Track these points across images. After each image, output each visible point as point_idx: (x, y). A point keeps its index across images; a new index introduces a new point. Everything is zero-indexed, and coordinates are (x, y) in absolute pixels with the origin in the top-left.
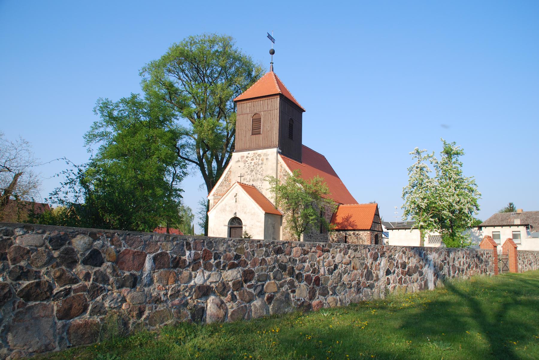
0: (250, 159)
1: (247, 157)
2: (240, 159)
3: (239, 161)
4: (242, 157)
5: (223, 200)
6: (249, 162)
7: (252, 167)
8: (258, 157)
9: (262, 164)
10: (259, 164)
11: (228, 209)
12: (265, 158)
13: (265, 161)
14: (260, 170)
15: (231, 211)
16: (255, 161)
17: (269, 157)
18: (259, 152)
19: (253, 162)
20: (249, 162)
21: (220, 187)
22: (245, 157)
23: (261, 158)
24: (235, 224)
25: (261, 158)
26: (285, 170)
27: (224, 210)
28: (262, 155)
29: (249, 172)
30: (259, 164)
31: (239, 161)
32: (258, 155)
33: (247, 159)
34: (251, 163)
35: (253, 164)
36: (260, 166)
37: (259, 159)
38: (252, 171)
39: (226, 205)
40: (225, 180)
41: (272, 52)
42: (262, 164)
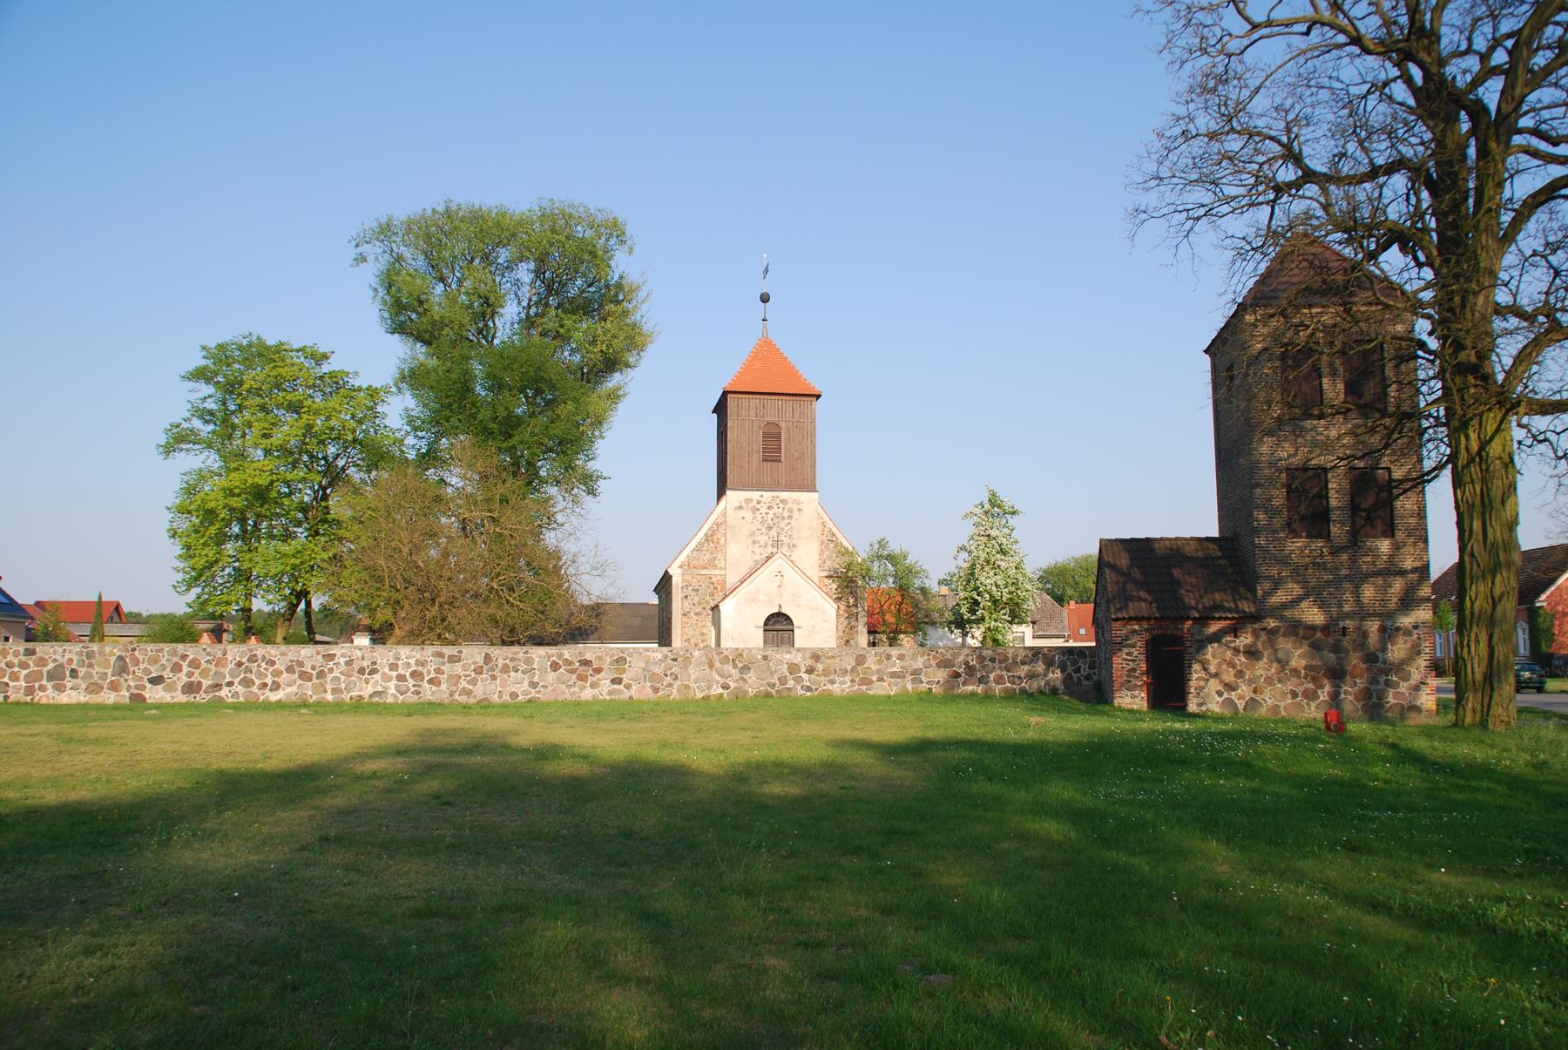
3: (740, 507)
4: (749, 501)
11: (762, 597)
12: (795, 508)
13: (795, 513)
16: (775, 510)
18: (784, 495)
24: (778, 625)
31: (740, 507)
38: (770, 528)
41: (765, 299)
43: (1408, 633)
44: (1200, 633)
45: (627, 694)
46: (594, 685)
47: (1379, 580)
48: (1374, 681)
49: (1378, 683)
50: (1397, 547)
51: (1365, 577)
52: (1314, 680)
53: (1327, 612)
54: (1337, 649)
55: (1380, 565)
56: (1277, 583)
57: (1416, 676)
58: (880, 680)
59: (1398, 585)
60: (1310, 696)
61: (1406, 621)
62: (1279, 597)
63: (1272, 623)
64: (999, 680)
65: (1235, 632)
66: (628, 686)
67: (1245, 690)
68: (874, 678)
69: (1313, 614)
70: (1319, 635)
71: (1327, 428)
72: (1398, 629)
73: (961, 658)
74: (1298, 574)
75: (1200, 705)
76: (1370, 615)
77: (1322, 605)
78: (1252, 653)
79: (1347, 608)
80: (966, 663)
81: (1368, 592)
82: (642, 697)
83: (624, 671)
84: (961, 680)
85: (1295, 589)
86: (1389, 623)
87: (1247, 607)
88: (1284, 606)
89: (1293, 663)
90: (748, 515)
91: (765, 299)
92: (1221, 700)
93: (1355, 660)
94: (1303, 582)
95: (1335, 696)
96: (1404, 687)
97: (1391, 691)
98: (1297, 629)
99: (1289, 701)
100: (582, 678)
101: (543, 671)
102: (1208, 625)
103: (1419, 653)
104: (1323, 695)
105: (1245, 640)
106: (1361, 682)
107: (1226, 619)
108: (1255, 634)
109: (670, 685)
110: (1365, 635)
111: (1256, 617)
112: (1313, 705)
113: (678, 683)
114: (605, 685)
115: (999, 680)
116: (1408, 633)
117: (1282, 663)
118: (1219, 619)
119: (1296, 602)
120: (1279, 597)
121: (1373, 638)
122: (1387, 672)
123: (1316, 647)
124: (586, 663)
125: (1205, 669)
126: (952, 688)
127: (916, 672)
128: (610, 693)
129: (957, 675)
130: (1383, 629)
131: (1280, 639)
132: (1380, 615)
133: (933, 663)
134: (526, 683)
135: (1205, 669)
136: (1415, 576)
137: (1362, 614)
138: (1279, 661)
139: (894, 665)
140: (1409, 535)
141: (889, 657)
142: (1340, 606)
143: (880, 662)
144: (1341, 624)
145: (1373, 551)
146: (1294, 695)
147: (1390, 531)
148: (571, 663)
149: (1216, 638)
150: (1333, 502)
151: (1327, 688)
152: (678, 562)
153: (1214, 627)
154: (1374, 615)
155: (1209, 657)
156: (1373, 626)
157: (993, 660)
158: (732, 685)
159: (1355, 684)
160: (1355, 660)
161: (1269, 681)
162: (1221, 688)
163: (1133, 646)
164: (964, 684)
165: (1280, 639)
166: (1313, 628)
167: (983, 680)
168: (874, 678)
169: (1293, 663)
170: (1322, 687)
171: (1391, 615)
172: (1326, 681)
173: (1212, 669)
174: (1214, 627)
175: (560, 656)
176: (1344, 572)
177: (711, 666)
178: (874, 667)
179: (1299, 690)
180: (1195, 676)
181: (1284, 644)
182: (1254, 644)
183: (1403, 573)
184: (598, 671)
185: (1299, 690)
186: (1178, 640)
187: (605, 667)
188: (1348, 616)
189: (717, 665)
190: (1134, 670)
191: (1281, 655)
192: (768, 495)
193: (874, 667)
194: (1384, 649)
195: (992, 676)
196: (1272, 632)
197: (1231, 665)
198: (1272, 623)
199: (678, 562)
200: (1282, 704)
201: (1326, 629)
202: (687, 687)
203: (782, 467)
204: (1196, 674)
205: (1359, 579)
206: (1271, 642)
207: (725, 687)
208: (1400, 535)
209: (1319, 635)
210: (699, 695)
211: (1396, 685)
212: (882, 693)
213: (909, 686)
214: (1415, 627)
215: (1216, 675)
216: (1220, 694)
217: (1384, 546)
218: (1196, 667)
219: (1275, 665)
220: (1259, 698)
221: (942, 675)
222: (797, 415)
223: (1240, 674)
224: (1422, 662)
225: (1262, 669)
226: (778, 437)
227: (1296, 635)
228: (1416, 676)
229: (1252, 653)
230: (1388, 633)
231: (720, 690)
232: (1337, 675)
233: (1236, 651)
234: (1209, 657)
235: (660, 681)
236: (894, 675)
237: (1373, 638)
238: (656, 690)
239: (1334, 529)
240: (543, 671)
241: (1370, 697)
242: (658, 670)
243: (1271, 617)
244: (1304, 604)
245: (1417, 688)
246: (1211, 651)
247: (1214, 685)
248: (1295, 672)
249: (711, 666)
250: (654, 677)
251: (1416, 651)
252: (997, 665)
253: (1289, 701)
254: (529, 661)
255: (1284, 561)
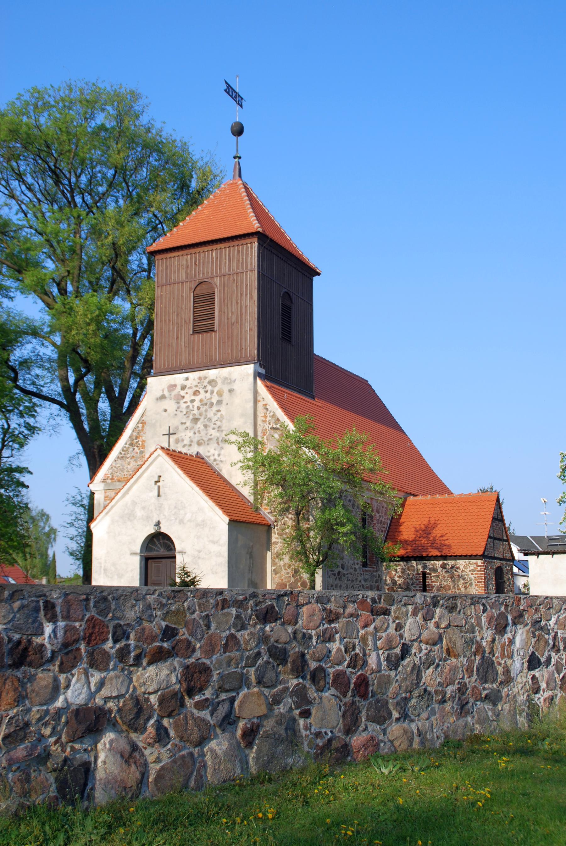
0: (190, 392)
1: (183, 388)
2: (166, 393)
3: (163, 397)
4: (172, 387)
5: (127, 493)
6: (188, 398)
7: (196, 411)
8: (209, 388)
9: (219, 402)
10: (212, 404)
11: (139, 513)
12: (226, 389)
13: (226, 395)
14: (215, 418)
15: (148, 518)
16: (202, 395)
17: (235, 386)
18: (212, 373)
19: (197, 398)
20: (188, 398)
21: (119, 461)
22: (179, 388)
23: (216, 390)
25: (216, 390)
26: (274, 416)
27: (129, 516)
28: (219, 382)
29: (188, 424)
30: (212, 404)
31: (163, 397)
32: (210, 382)
33: (183, 393)
34: (193, 401)
35: (197, 404)
36: (215, 408)
37: (212, 392)
39: (134, 503)
40: (131, 444)
41: (238, 131)
42: (219, 402)
90: (170, 405)
91: (238, 131)
192: (193, 376)
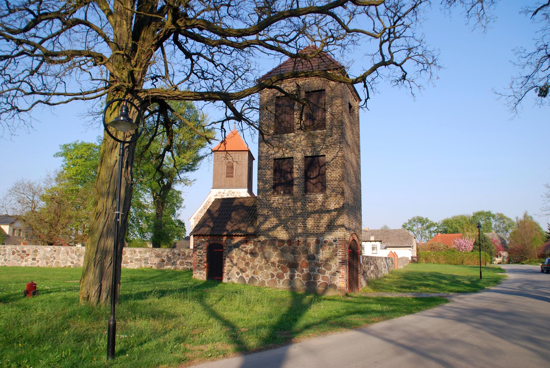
43: (331, 244)
44: (230, 242)
45: (36, 265)
46: (26, 261)
47: (317, 216)
48: (312, 270)
49: (315, 271)
50: (326, 197)
51: (309, 214)
52: (282, 268)
53: (289, 233)
54: (293, 252)
55: (317, 208)
56: (266, 218)
57: (334, 268)
58: (131, 262)
59: (326, 219)
60: (280, 277)
61: (329, 238)
62: (267, 225)
63: (262, 238)
64: (182, 264)
65: (246, 242)
66: (38, 261)
67: (249, 273)
68: (129, 261)
69: (282, 234)
70: (286, 244)
71: (295, 137)
72: (325, 242)
73: (165, 253)
74: (276, 212)
75: (229, 279)
76: (311, 234)
77: (286, 228)
78: (253, 254)
79: (300, 231)
80: (167, 256)
81: (310, 223)
82: (42, 266)
83: (36, 255)
84: (165, 263)
85: (274, 221)
86: (321, 239)
87: (251, 230)
88: (269, 230)
89: (272, 260)
92: (238, 277)
93: (302, 259)
94: (278, 217)
95: (292, 277)
96: (328, 274)
97: (321, 275)
98: (274, 241)
99: (270, 279)
100: (22, 258)
101: (9, 254)
102: (232, 239)
103: (336, 255)
104: (286, 277)
105: (250, 247)
106: (306, 270)
107: (241, 236)
108: (255, 244)
109: (52, 261)
110: (308, 245)
111: (255, 235)
112: (282, 281)
113: (55, 260)
114: (30, 262)
115: (182, 264)
116: (331, 244)
117: (267, 259)
118: (238, 236)
119: (275, 227)
120: (267, 225)
121: (312, 249)
122: (319, 265)
123: (283, 252)
124: (24, 252)
125: (232, 261)
126: (161, 266)
127: (146, 259)
128: (31, 264)
129: (163, 261)
130: (318, 242)
131: (267, 247)
132: (317, 234)
133: (154, 255)
134: (3, 259)
135: (232, 261)
136: (335, 213)
137: (307, 234)
138: (265, 258)
139: (137, 256)
140: (333, 191)
141: (135, 252)
142: (296, 229)
143: (131, 254)
144: (297, 239)
145: (315, 201)
146: (273, 276)
147: (323, 189)
148: (19, 252)
149: (237, 246)
150: (295, 175)
151: (289, 273)
152: (193, 217)
153: (237, 240)
154: (313, 234)
155: (234, 255)
156: (312, 241)
157: (179, 255)
158: (75, 262)
159: (303, 271)
160: (302, 259)
161: (261, 268)
162: (239, 271)
163: (201, 249)
164: (166, 265)
165: (267, 247)
166: (282, 241)
167: (174, 264)
168: (129, 261)
169: (272, 260)
170: (286, 272)
171: (322, 234)
172: (288, 269)
173: (235, 261)
174: (237, 240)
175: (16, 249)
176: (299, 211)
177: (68, 254)
178: (129, 256)
179: (275, 273)
180: (227, 264)
181: (269, 249)
182: (254, 249)
183: (329, 211)
184: (28, 255)
185: (275, 273)
186: (221, 246)
187: (30, 253)
188: (300, 235)
189: (70, 253)
190: (201, 260)
191: (266, 255)
193: (129, 256)
194: (317, 252)
195: (178, 262)
196: (264, 243)
197: (244, 259)
198: (262, 238)
199: (193, 217)
200: (266, 280)
201: (290, 242)
202: (58, 262)
203: (234, 179)
204: (227, 264)
205: (306, 215)
206: (262, 249)
207: (72, 263)
208: (328, 192)
209: (286, 244)
210: (63, 266)
211: (324, 272)
212: (132, 268)
213: (143, 265)
214: (335, 241)
215: (236, 265)
216: (238, 274)
217: (320, 197)
218: (227, 260)
219: (264, 260)
220: (255, 276)
221: (157, 261)
222: (240, 158)
223: (247, 264)
224: (338, 260)
225: (258, 261)
226: (232, 167)
227: (274, 244)
228: (334, 268)
229: (253, 254)
230: (320, 244)
231: (70, 264)
232: (293, 266)
233: (246, 253)
234: (234, 255)
235: (49, 259)
236: (137, 260)
237: (312, 249)
238: (47, 263)
239: (295, 189)
240: (9, 254)
241: (310, 279)
242: (48, 255)
243: (263, 235)
244: (279, 229)
245: (334, 274)
246: (235, 253)
247: (235, 270)
248: (273, 264)
249: (68, 254)
250: (47, 258)
251: (334, 254)
252: (181, 257)
253: (270, 279)
254: (5, 251)
255: (269, 206)
